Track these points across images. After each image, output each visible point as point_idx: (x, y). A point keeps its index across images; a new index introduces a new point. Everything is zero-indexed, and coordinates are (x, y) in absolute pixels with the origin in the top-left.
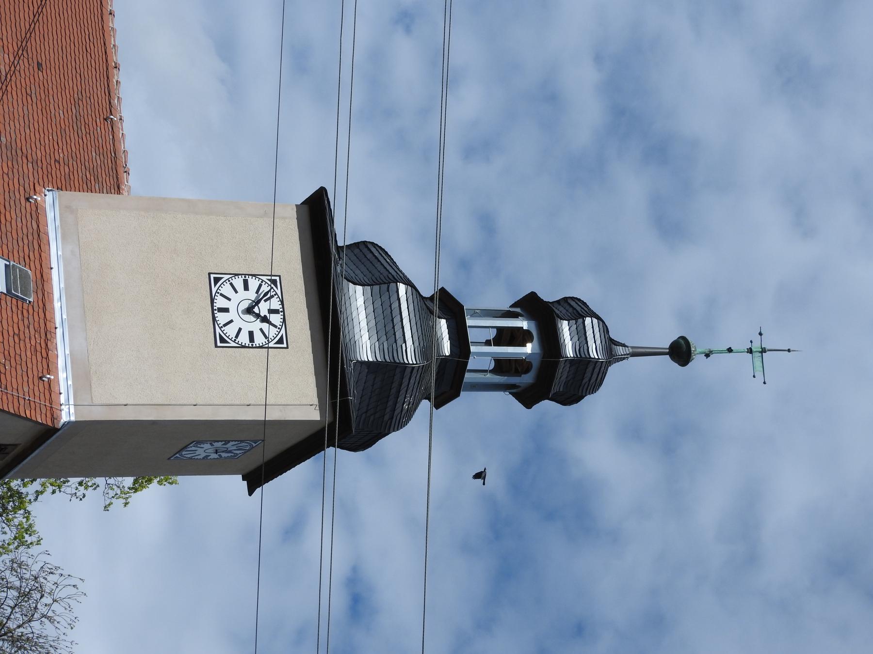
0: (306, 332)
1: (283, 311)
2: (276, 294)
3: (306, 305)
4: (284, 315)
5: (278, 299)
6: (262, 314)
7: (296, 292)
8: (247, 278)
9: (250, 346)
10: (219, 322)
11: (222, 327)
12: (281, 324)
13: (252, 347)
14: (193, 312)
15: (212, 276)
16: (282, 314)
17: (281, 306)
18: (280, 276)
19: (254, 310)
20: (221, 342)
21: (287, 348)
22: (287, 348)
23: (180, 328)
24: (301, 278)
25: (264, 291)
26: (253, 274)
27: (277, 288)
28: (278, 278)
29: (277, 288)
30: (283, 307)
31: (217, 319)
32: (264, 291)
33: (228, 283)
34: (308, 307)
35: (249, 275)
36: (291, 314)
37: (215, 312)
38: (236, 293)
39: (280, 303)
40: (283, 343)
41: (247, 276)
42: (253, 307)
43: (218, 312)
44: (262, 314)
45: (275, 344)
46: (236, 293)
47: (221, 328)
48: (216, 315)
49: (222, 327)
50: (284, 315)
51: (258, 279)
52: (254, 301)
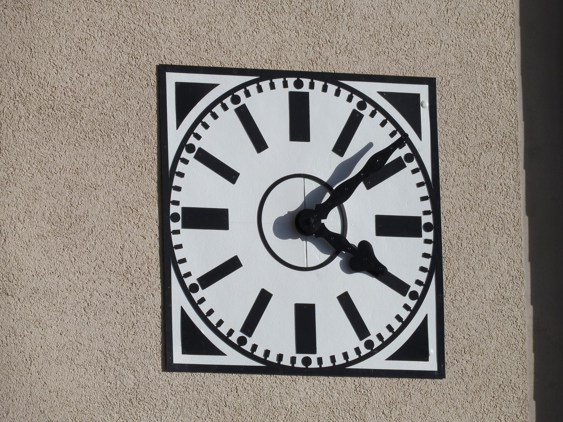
0: (517, 312)
1: (436, 227)
2: (414, 155)
3: (522, 203)
4: (437, 243)
5: (419, 178)
6: (353, 239)
7: (489, 146)
8: (300, 357)
9: (299, 364)
10: (183, 268)
11: (194, 288)
12: (423, 277)
13: (306, 372)
14: (88, 226)
15: (172, 79)
16: (430, 235)
17: (427, 205)
18: (431, 82)
19: (323, 221)
20: (186, 350)
21: (440, 374)
22: (440, 374)
23: (36, 290)
24: (514, 89)
25: (370, 146)
26: (330, 70)
27: (183, 313)
28: (423, 90)
29: (183, 313)
30: (436, 211)
31: (179, 254)
32: (370, 146)
33: (232, 107)
34: (531, 210)
35: (313, 76)
36: (464, 235)
37: (175, 226)
38: (233, 181)
39: (424, 191)
40: (424, 357)
41: (306, 82)
42: (324, 211)
43: (184, 226)
44: (353, 239)
45: (211, 87)
46: (233, 181)
47: (189, 291)
48: (176, 240)
49: (194, 288)
50: (437, 243)
51: (345, 93)
52: (326, 186)
